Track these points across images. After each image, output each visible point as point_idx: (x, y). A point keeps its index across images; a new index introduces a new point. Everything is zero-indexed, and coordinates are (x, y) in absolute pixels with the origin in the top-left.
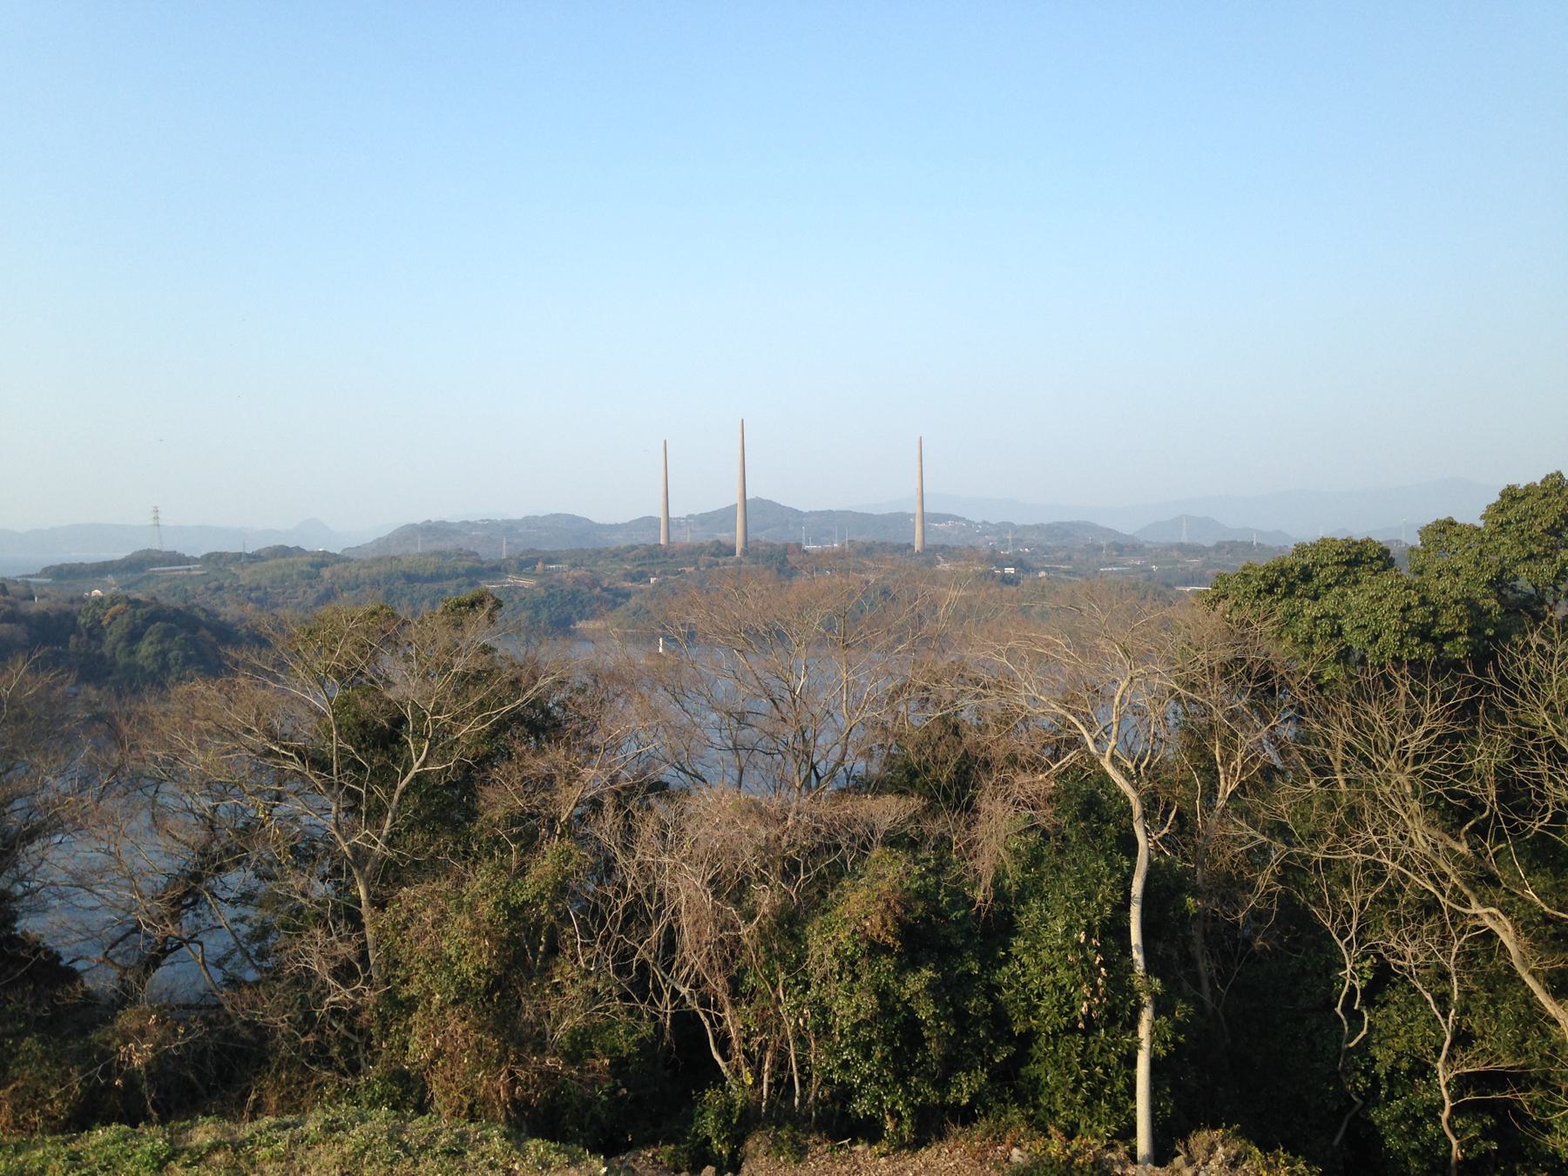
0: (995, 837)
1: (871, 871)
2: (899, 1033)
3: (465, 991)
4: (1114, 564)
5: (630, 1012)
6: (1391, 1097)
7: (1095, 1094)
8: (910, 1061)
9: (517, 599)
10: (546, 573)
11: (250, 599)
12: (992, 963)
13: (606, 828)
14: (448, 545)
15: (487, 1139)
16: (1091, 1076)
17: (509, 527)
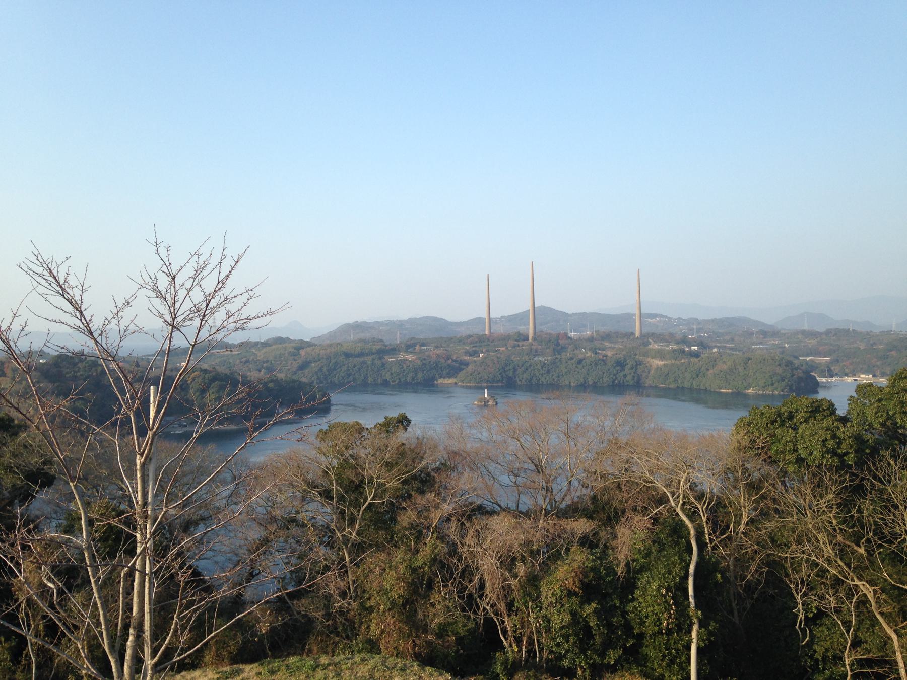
0: (629, 539)
1: (571, 557)
2: (581, 632)
3: (393, 604)
4: (761, 343)
5: (465, 616)
6: (824, 669)
7: (672, 662)
8: (587, 644)
9: (405, 367)
10: (421, 351)
11: (263, 367)
12: (625, 600)
13: (452, 530)
14: (367, 335)
15: (413, 666)
16: (670, 654)
17: (400, 325)
